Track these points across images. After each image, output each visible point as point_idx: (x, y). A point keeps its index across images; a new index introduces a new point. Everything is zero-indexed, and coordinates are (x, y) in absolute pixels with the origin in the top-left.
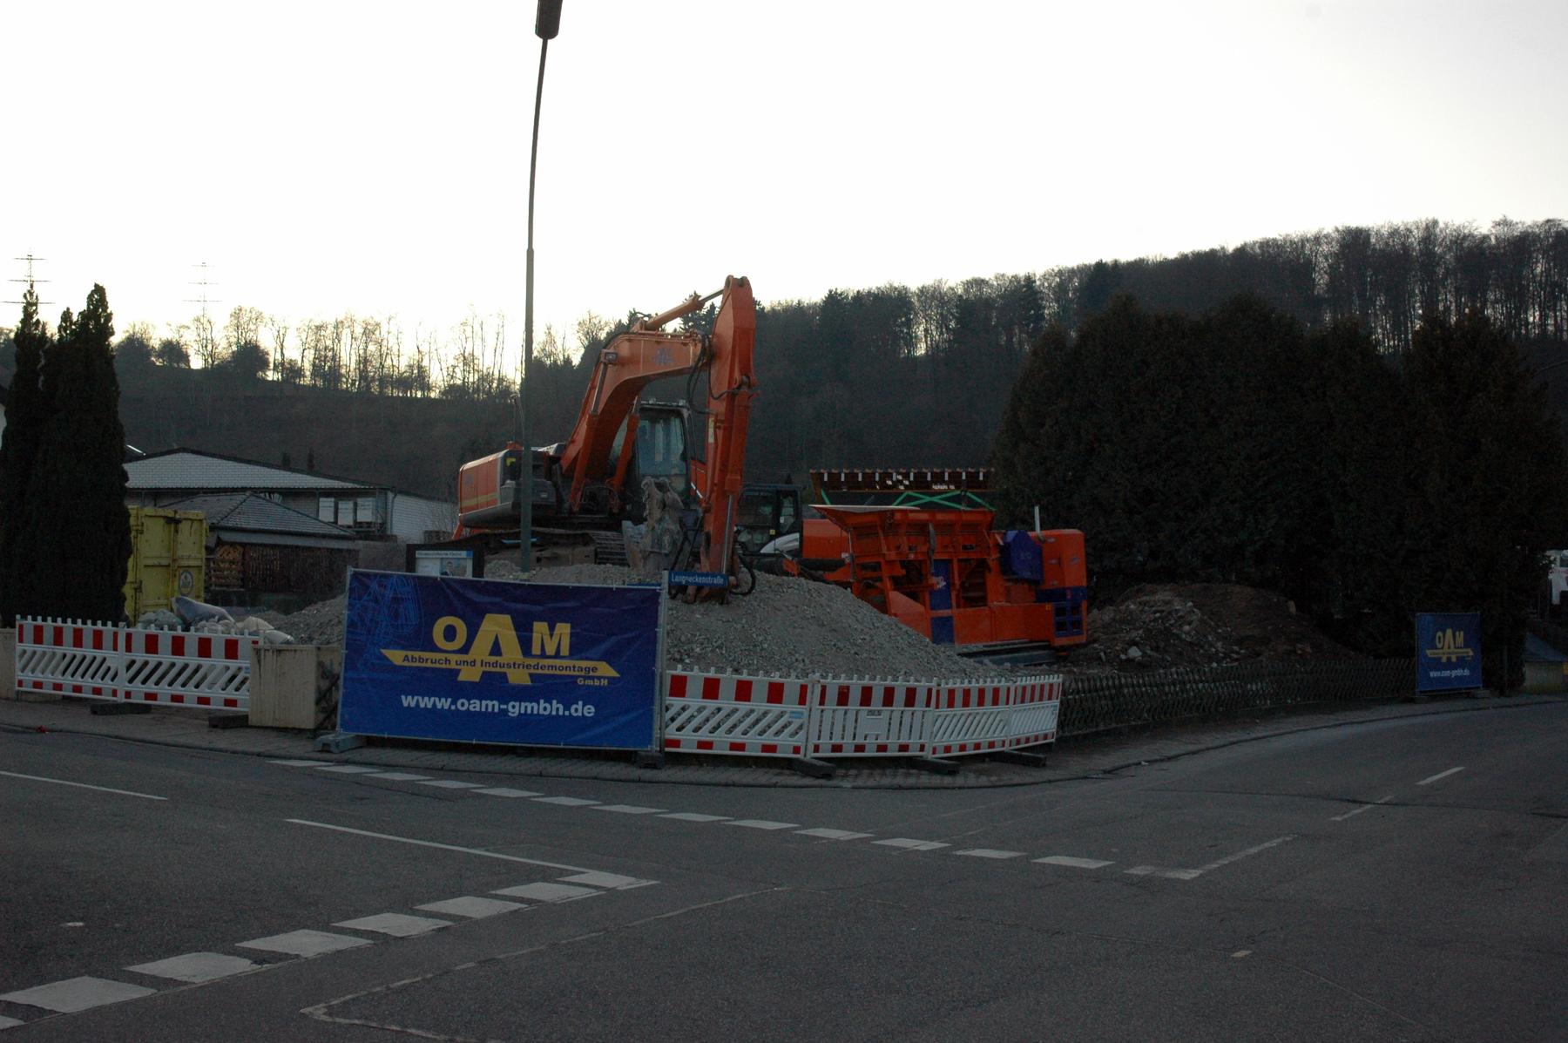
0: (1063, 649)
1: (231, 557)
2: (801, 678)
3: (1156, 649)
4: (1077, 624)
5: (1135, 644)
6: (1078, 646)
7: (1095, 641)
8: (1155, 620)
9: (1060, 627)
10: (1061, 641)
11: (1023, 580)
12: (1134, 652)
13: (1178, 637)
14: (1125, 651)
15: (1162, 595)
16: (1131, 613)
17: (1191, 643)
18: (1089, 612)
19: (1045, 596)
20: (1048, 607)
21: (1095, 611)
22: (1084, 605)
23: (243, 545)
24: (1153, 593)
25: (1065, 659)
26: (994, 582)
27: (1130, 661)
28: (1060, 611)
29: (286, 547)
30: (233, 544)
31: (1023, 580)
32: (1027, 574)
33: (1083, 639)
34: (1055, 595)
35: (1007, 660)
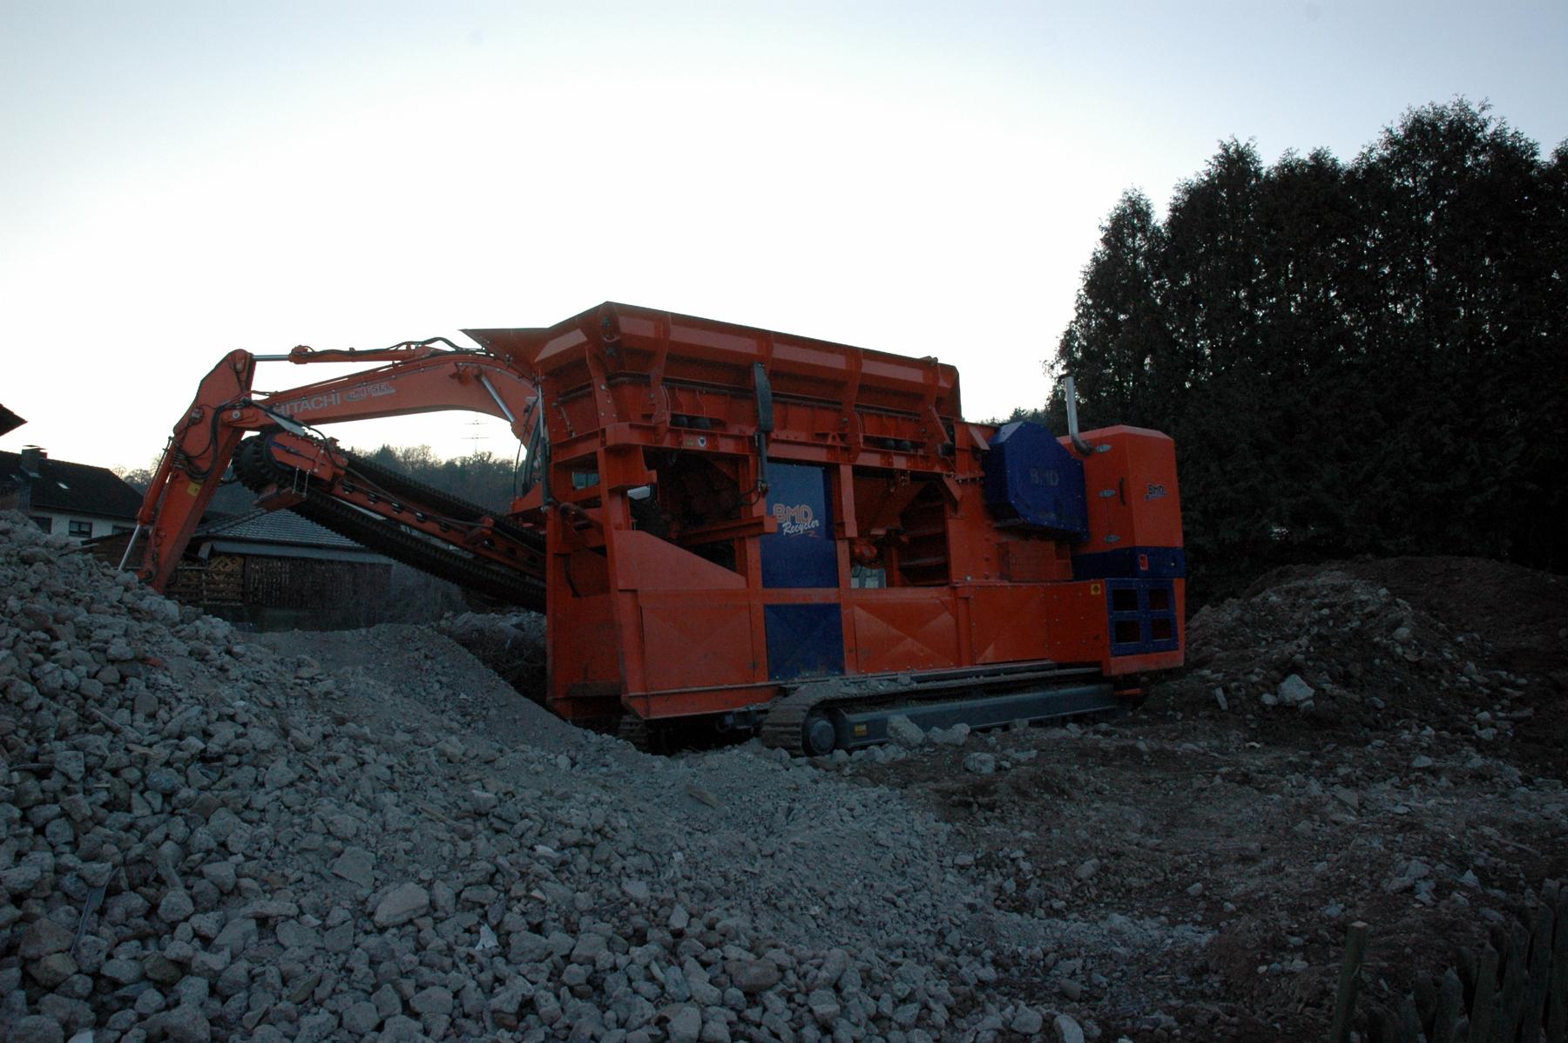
0: (1130, 680)
1: (228, 569)
2: (385, 781)
3: (1346, 680)
4: (1164, 628)
5: (1289, 668)
6: (1171, 673)
7: (1202, 663)
8: (1321, 621)
9: (1124, 632)
10: (1121, 665)
11: (1043, 533)
12: (1296, 689)
13: (1387, 653)
14: (1273, 686)
15: (1329, 577)
16: (1272, 610)
17: (1418, 666)
18: (1191, 611)
19: (1086, 567)
20: (1096, 588)
21: (1206, 609)
22: (1179, 587)
23: (243, 556)
24: (1183, 735)
25: (1137, 702)
26: (965, 538)
27: (1287, 709)
28: (1122, 599)
29: (294, 559)
30: (229, 555)
31: (1043, 533)
32: (1049, 518)
33: (1177, 659)
34: (1120, 563)
35: (963, 716)
